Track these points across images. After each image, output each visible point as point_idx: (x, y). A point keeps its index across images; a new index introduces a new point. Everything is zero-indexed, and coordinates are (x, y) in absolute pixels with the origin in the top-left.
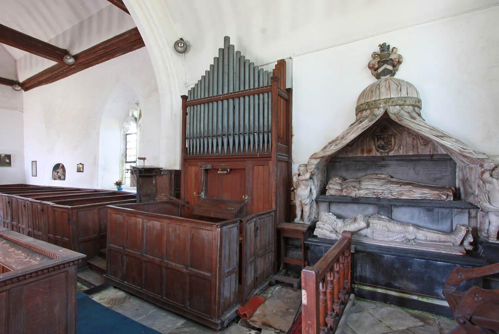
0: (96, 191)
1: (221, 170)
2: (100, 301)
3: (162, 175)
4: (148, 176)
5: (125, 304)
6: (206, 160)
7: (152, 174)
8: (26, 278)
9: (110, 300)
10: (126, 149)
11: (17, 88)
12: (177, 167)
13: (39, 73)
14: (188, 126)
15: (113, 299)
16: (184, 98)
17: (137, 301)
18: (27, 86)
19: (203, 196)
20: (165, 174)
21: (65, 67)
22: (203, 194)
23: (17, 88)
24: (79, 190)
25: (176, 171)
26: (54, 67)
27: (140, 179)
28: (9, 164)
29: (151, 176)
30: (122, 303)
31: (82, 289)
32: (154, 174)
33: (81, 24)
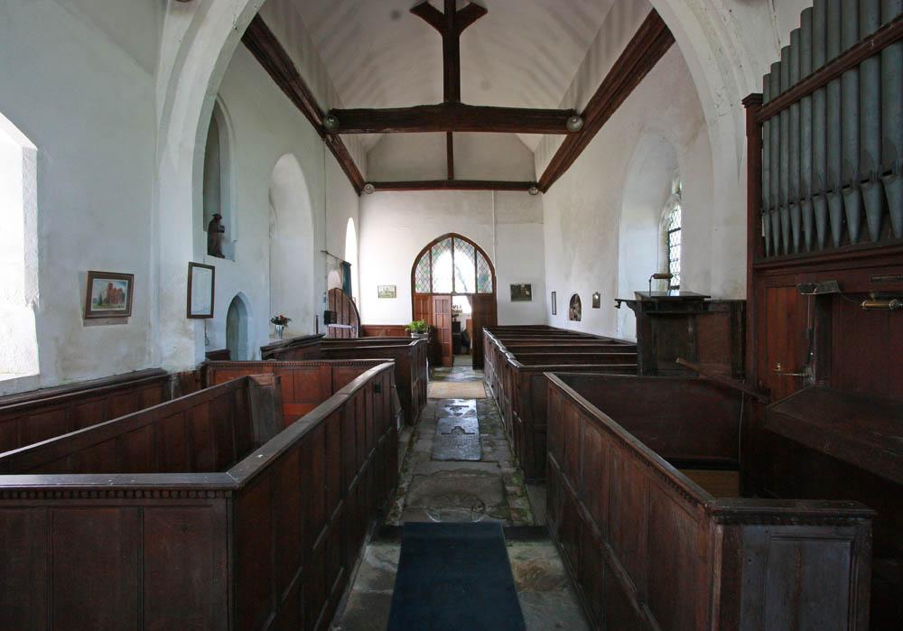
0: (613, 341)
1: (877, 299)
2: (515, 561)
3: (712, 313)
4: (675, 317)
5: (545, 596)
6: (821, 267)
7: (685, 312)
8: (194, 493)
9: (533, 569)
10: (669, 261)
11: (534, 192)
12: (742, 295)
13: (573, 162)
14: (766, 175)
15: (539, 569)
16: (752, 102)
17: (573, 605)
18: (543, 186)
19: (813, 379)
20: (719, 312)
21: (576, 138)
22: (810, 373)
23: (534, 192)
24: (593, 337)
25: (738, 302)
26: (566, 140)
27: (654, 323)
28: (529, 298)
29: (684, 317)
30: (544, 590)
31: (524, 518)
32: (690, 310)
33: (588, 55)
